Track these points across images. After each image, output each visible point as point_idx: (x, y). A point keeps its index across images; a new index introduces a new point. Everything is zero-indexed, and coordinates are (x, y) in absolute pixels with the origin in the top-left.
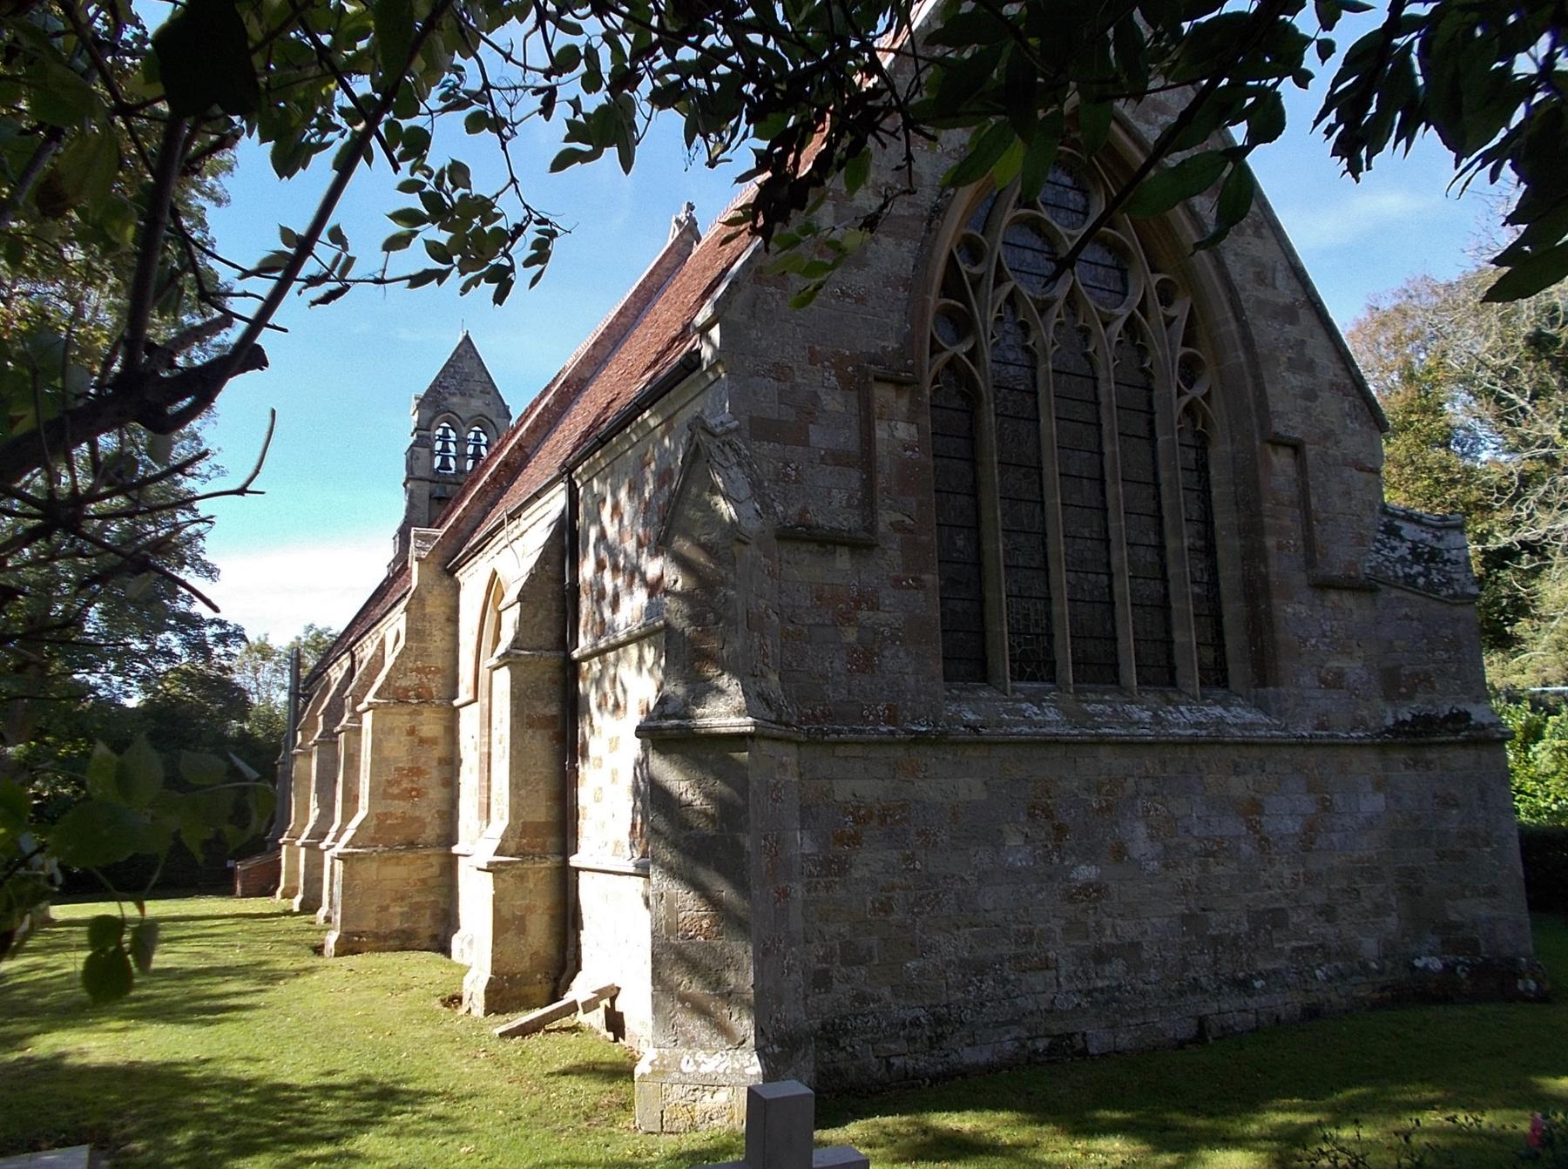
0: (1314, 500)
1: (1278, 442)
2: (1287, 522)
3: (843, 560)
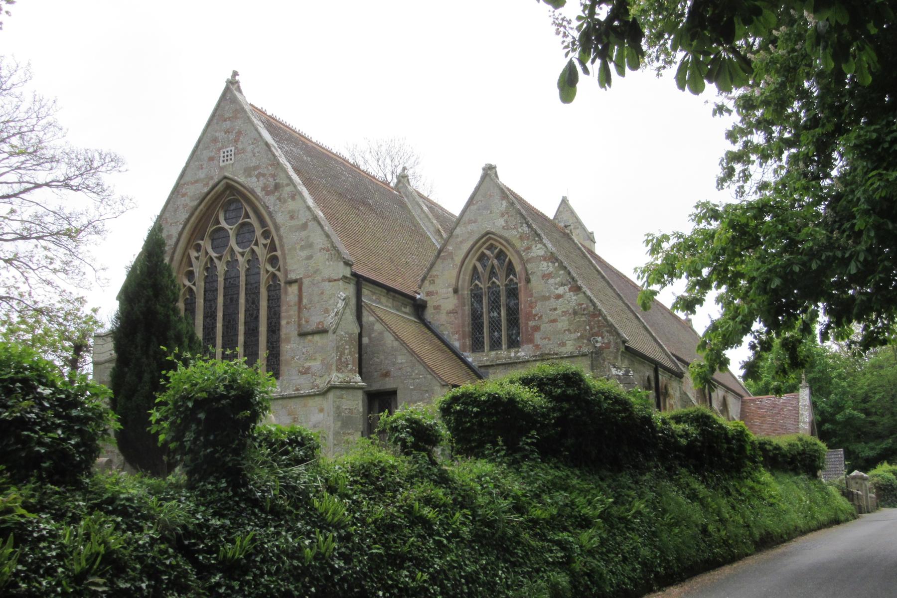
0: (305, 301)
1: (290, 283)
2: (292, 313)
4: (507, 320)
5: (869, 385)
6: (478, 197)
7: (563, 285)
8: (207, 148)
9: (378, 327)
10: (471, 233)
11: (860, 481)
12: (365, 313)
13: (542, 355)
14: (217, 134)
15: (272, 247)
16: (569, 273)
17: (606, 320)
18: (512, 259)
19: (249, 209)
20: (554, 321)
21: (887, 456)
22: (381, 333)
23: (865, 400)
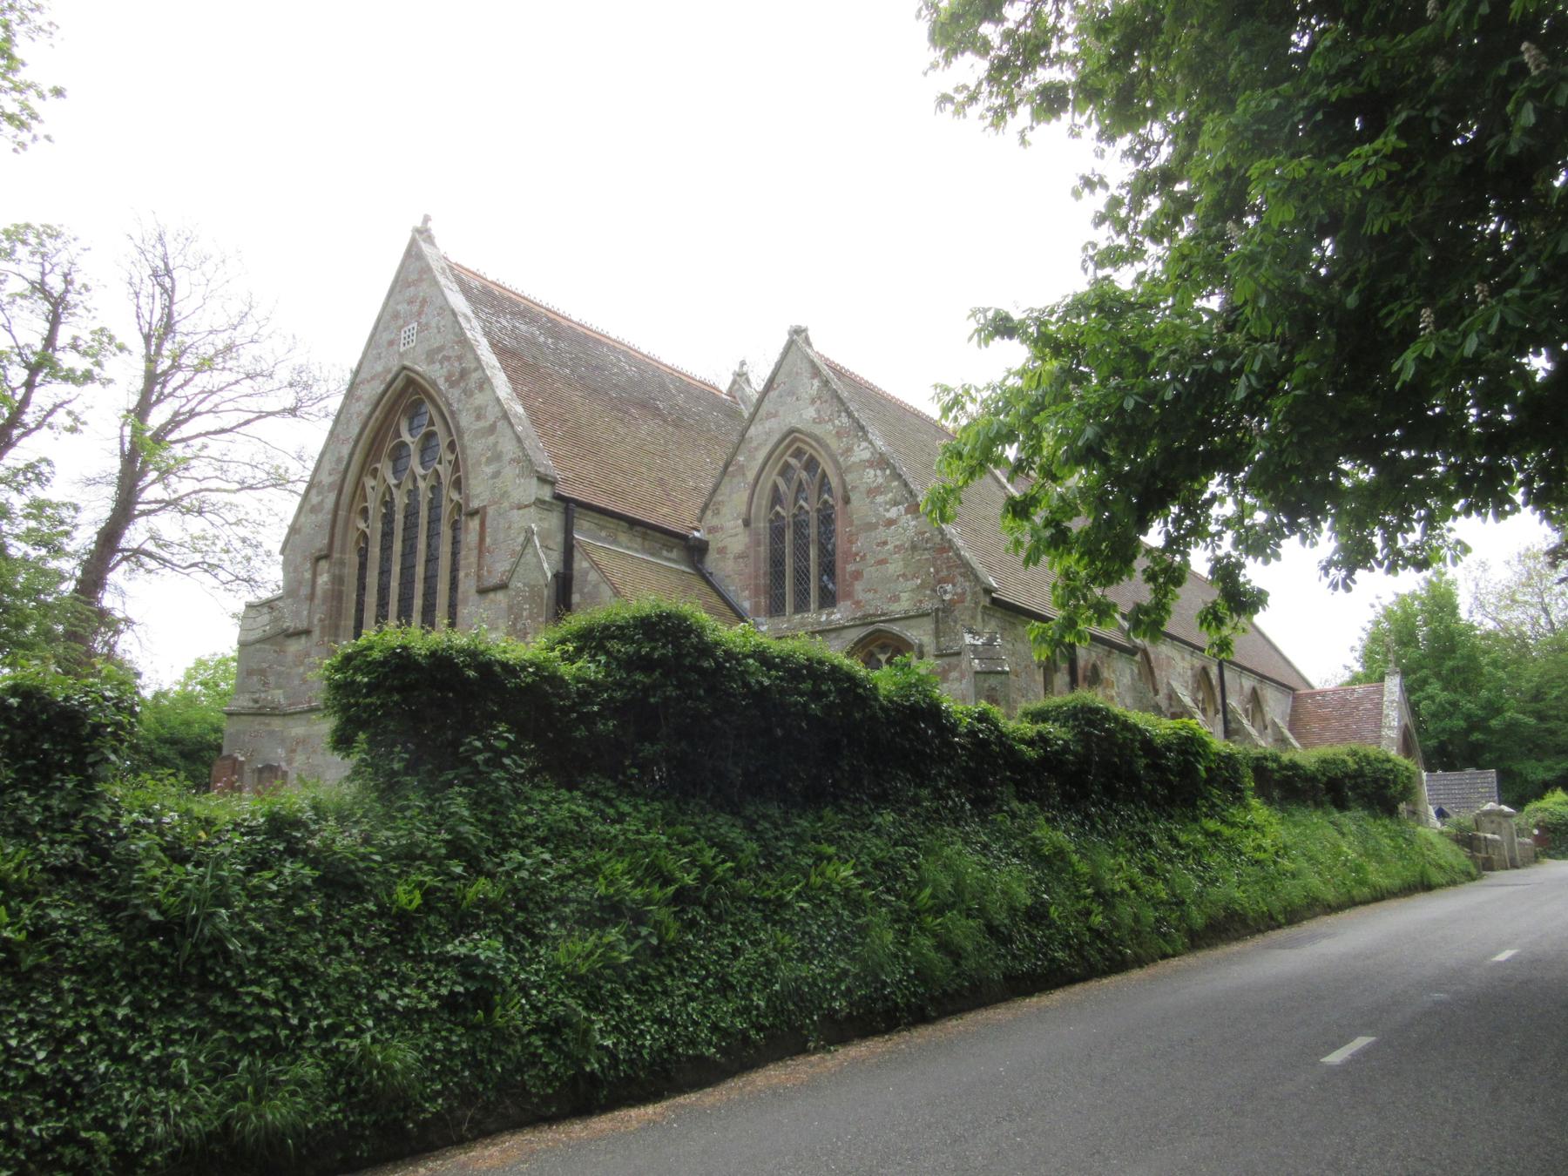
0: (488, 540)
4: (820, 565)
5: (1541, 676)
6: (780, 378)
7: (896, 504)
8: (386, 329)
9: (593, 576)
10: (768, 434)
11: (1497, 819)
12: (577, 556)
13: (865, 616)
14: (399, 307)
15: (456, 466)
16: (906, 485)
17: (959, 556)
18: (828, 472)
19: (434, 412)
20: (883, 562)
21: (1567, 782)
22: (596, 586)
23: (1537, 696)
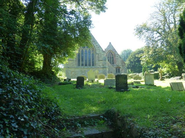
3: (72, 61)
15: (93, 49)
